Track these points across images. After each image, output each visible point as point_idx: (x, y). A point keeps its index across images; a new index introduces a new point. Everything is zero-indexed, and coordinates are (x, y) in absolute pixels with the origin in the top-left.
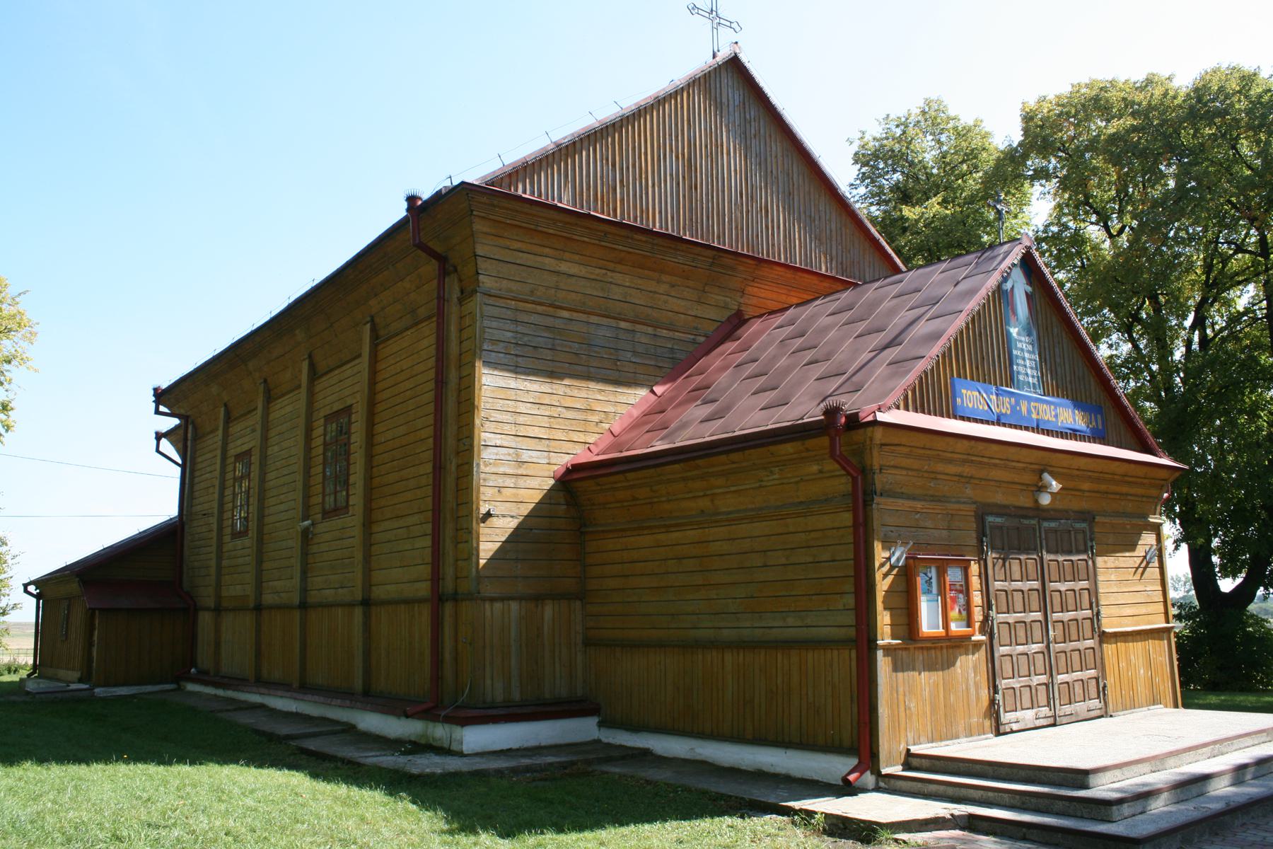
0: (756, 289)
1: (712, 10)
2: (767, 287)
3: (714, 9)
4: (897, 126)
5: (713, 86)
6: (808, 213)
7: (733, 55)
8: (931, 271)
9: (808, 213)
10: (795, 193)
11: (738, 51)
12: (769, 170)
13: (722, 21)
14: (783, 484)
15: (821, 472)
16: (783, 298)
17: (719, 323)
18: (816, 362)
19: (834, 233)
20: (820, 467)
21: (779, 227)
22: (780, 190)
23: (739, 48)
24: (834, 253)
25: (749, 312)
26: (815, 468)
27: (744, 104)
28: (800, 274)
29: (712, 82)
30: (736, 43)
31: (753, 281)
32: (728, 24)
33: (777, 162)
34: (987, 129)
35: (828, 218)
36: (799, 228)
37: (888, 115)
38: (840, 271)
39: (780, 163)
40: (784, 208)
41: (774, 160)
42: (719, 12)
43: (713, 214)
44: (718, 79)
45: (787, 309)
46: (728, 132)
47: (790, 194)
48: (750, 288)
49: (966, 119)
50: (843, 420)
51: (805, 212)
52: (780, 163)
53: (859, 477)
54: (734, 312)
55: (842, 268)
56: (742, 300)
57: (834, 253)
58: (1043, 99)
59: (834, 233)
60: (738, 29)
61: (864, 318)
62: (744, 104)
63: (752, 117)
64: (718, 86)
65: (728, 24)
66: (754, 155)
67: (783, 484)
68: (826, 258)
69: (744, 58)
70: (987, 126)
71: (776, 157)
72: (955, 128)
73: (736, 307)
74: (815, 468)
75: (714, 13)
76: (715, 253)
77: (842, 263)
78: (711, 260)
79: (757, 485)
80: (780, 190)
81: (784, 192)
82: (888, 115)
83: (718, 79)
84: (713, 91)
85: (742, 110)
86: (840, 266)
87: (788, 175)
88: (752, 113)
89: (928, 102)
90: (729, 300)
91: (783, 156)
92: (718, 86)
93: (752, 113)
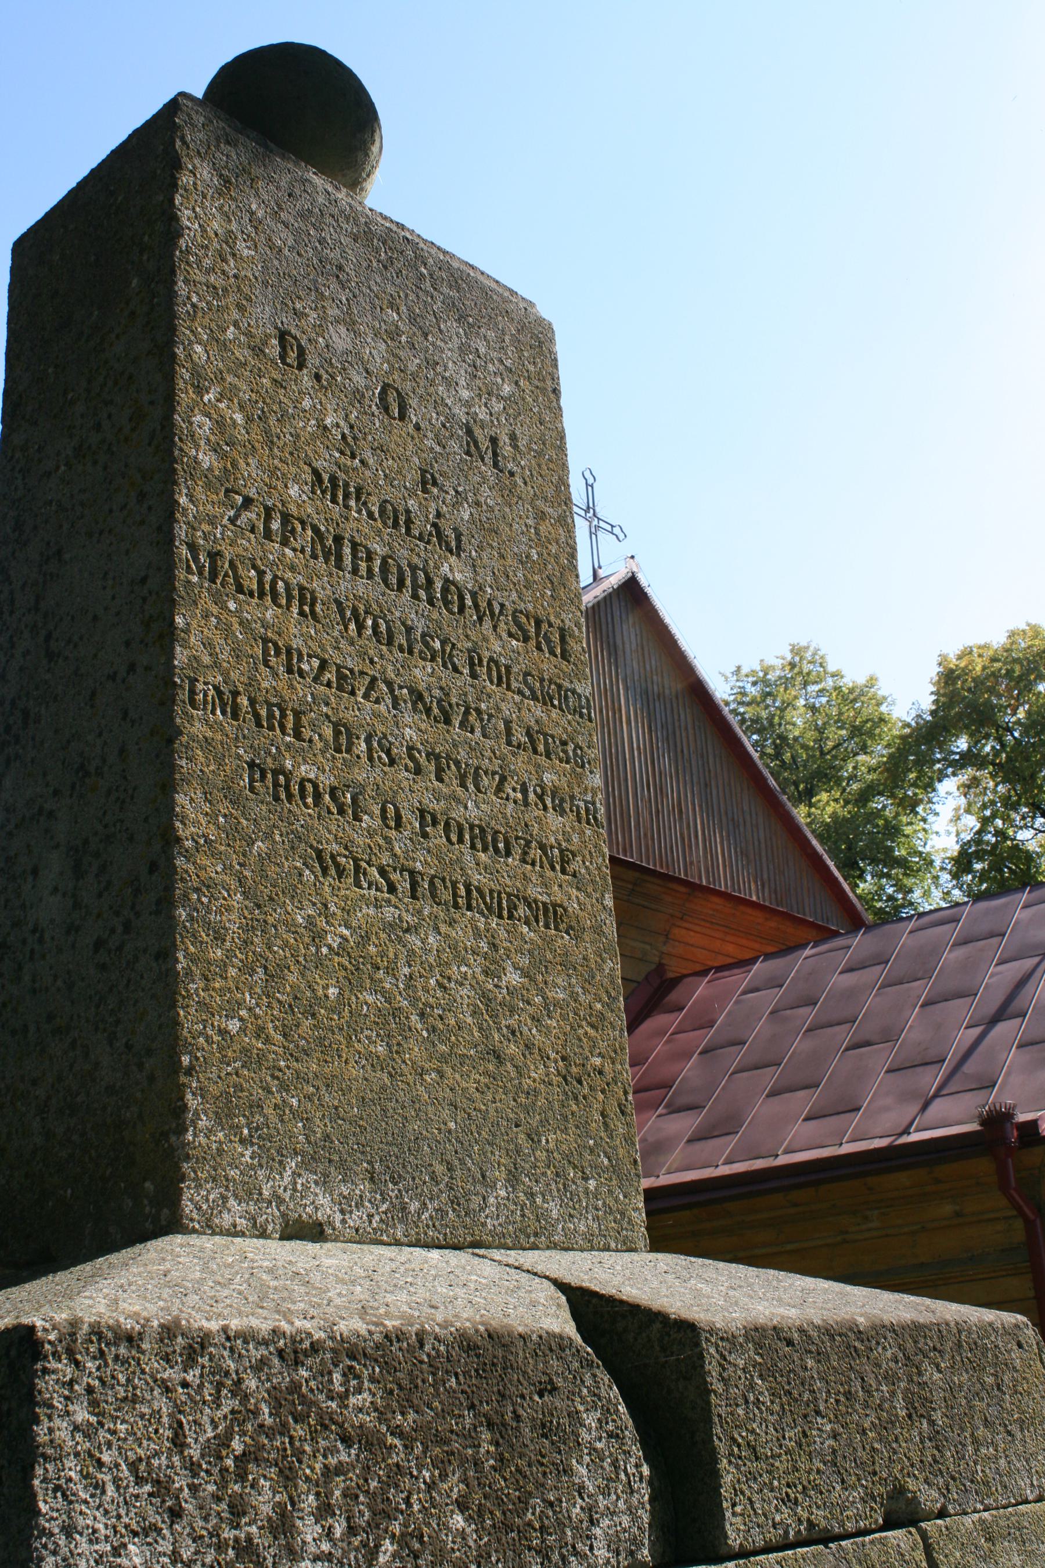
0: (683, 932)
1: (588, 507)
2: (698, 929)
3: (591, 505)
4: (754, 684)
5: (603, 620)
6: (730, 816)
7: (630, 574)
8: (1006, 905)
9: (730, 816)
10: (713, 783)
11: (635, 569)
12: (679, 750)
13: (602, 524)
14: (887, 1236)
15: (958, 1214)
16: (730, 949)
17: (635, 985)
18: (868, 1044)
19: (763, 846)
20: (957, 1208)
21: (696, 837)
22: (695, 780)
23: (637, 565)
24: (765, 876)
25: (674, 968)
26: (948, 1209)
27: (643, 649)
28: (742, 908)
29: (602, 614)
30: (632, 557)
31: (682, 919)
32: (609, 528)
33: (688, 738)
34: (880, 693)
35: (754, 822)
36: (721, 837)
37: (739, 668)
38: (773, 901)
39: (691, 738)
40: (701, 806)
41: (684, 734)
42: (597, 509)
43: (615, 814)
44: (609, 610)
45: (753, 961)
46: (626, 689)
47: (706, 785)
48: (676, 931)
49: (854, 676)
50: (1015, 1133)
51: (726, 814)
52: (691, 738)
53: (1038, 1221)
54: (653, 966)
55: (776, 898)
56: (664, 949)
57: (765, 876)
58: (967, 652)
59: (763, 846)
60: (621, 536)
61: (919, 975)
62: (643, 649)
63: (654, 667)
64: (609, 620)
65: (609, 528)
66: (659, 727)
67: (887, 1236)
68: (756, 882)
69: (643, 580)
70: (883, 689)
71: (686, 729)
72: (837, 688)
73: (657, 959)
74: (948, 1209)
75: (591, 511)
76: (637, 875)
77: (776, 892)
78: (630, 886)
79: (839, 1238)
80: (695, 780)
81: (699, 783)
82: (739, 668)
83: (609, 610)
84: (604, 627)
85: (641, 658)
86: (773, 896)
87: (702, 757)
88: (653, 662)
89: (797, 651)
90: (648, 947)
91: (694, 728)
92: (609, 620)
93: (653, 662)
